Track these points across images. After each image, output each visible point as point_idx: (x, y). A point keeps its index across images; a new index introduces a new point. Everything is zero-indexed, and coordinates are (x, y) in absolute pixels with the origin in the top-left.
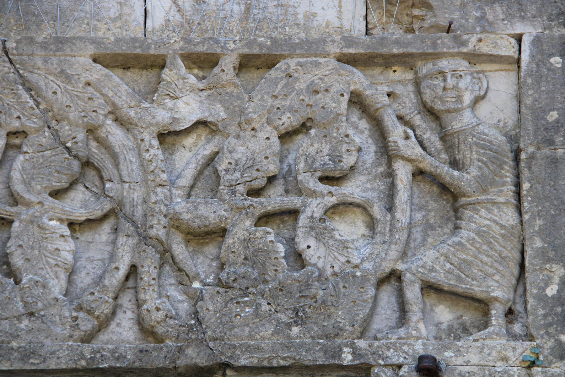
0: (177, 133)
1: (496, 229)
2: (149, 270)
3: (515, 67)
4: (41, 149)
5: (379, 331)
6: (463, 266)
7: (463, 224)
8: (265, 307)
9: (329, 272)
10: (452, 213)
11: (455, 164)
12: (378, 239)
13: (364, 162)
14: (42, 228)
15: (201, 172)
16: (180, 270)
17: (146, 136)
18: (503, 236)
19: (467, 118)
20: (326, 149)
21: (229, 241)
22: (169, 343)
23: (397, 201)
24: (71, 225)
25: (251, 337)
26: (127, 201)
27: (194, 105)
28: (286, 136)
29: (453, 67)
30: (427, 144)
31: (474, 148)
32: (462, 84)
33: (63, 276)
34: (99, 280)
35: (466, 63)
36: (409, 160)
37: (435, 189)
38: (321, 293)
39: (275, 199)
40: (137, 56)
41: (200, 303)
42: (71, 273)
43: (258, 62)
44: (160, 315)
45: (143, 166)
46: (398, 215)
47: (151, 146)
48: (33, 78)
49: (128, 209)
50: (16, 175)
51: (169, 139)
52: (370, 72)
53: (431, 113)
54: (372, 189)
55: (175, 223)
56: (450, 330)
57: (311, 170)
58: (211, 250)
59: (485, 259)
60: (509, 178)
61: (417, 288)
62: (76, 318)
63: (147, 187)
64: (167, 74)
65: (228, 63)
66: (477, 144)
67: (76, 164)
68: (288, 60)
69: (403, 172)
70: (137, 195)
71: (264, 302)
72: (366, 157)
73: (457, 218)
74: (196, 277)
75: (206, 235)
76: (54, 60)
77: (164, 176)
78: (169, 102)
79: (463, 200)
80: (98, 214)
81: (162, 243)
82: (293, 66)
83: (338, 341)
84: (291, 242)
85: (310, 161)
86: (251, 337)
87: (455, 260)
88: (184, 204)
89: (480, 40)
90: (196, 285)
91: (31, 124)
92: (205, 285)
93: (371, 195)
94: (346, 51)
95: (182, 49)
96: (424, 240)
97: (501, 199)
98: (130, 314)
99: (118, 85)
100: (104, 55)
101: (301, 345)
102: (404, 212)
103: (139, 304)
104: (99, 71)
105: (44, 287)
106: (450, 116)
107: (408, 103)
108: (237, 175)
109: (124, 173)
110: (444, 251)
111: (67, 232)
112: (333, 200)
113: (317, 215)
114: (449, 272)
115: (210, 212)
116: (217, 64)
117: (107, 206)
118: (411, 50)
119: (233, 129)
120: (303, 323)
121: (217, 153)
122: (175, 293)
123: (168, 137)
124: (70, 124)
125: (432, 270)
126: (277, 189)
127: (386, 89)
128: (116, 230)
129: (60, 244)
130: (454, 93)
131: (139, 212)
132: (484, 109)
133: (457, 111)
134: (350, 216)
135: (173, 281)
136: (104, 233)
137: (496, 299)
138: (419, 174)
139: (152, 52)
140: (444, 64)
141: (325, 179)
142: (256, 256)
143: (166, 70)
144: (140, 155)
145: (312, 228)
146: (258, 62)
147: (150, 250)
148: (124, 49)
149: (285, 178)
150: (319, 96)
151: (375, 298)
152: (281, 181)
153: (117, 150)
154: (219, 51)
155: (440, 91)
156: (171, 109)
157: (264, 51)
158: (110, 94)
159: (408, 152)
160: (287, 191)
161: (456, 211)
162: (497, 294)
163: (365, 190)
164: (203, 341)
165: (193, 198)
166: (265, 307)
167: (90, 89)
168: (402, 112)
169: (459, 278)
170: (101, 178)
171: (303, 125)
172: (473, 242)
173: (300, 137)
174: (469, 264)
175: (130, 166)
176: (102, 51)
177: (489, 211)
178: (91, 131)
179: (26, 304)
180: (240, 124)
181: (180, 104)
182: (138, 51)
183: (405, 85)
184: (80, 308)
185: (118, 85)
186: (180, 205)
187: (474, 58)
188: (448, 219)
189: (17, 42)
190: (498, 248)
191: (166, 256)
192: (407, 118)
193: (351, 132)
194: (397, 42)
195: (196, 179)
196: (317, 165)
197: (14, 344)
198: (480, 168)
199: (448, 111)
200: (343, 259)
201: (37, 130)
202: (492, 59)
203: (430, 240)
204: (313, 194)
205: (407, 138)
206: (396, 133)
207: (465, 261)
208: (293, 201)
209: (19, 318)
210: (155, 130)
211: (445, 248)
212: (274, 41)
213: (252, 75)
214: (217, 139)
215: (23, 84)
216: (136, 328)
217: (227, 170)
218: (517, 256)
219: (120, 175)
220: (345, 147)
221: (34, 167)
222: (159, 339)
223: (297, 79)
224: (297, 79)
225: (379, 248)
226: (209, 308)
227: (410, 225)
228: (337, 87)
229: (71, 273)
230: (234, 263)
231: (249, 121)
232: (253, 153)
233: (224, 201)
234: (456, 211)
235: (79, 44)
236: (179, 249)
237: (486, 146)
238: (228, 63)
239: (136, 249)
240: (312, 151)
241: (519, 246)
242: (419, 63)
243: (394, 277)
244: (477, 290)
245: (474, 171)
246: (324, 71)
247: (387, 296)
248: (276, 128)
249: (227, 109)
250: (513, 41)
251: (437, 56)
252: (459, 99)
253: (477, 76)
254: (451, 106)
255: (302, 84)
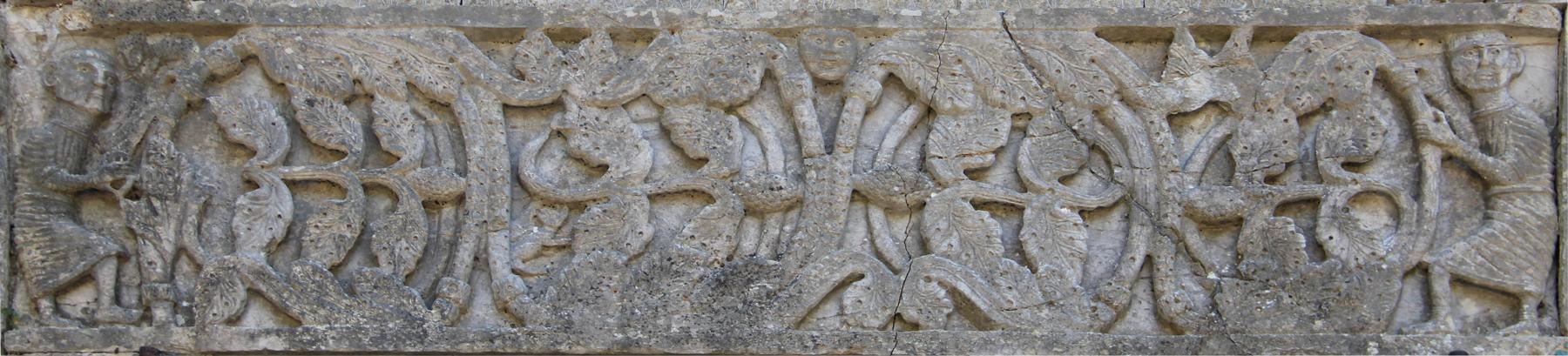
0: (1185, 114)
1: (1533, 220)
2: (1165, 261)
3: (1555, 40)
4: (1048, 132)
5: (1403, 324)
6: (1496, 259)
7: (1496, 214)
8: (1287, 300)
9: (1353, 264)
10: (1482, 202)
11: (1486, 148)
12: (1404, 229)
13: (1387, 146)
14: (1054, 216)
15: (1211, 157)
16: (1195, 260)
17: (1155, 117)
18: (1539, 227)
19: (1503, 98)
20: (1349, 132)
21: (1247, 231)
22: (1188, 334)
23: (1426, 190)
24: (1082, 212)
25: (1273, 330)
26: (1139, 188)
27: (1206, 83)
28: (1303, 118)
29: (1489, 41)
30: (1457, 126)
31: (1511, 132)
32: (1499, 61)
33: (1078, 266)
34: (1114, 271)
35: (1503, 37)
36: (1439, 145)
37: (1464, 175)
38: (1345, 286)
39: (1293, 187)
40: (1143, 29)
41: (1218, 295)
42: (1086, 261)
43: (1272, 35)
44: (1179, 307)
45: (1155, 150)
46: (1427, 205)
47: (1162, 129)
48: (1034, 54)
49: (1140, 196)
50: (1024, 160)
51: (1177, 121)
52: (1394, 46)
53: (1461, 91)
54: (1396, 176)
55: (1190, 212)
56: (1477, 323)
57: (1333, 155)
58: (1225, 239)
59: (1519, 251)
60: (1547, 166)
61: (1446, 281)
62: (1095, 309)
63: (1159, 173)
64: (1176, 49)
65: (1242, 36)
66: (1513, 128)
67: (1084, 147)
68: (1307, 33)
69: (1432, 157)
70: (1149, 181)
71: (1285, 295)
72: (1389, 140)
73: (1487, 207)
74: (1212, 268)
75: (1213, 225)
76: (1056, 35)
77: (1176, 162)
78: (1178, 80)
79: (1497, 189)
80: (1110, 201)
81: (1176, 232)
82: (1313, 40)
83: (1364, 335)
84: (1311, 232)
85: (1332, 146)
86: (1273, 330)
87: (1487, 253)
88: (1198, 191)
89: (1520, 11)
90: (1212, 276)
91: (1036, 105)
92: (1222, 276)
93: (1395, 182)
94: (1372, 22)
95: (1191, 20)
96: (1451, 231)
97: (1538, 188)
98: (1145, 305)
99: (1124, 62)
100: (1107, 29)
101: (1325, 339)
102: (1433, 201)
103: (1155, 295)
104: (1102, 48)
105: (1061, 277)
106: (1484, 96)
107: (1437, 80)
108: (1254, 160)
109: (1135, 158)
110: (1476, 242)
111: (1080, 221)
112: (1358, 188)
113: (1340, 204)
114: (1481, 265)
115: (1227, 201)
116: (1228, 37)
117: (1119, 193)
118: (1443, 22)
119: (1247, 110)
120: (1327, 316)
121: (1229, 136)
122: (1188, 283)
123: (1178, 118)
124: (1075, 105)
125: (1462, 263)
126: (1295, 174)
127: (1415, 65)
128: (1127, 218)
129: (1074, 233)
130: (1489, 71)
131: (1152, 199)
132: (1520, 88)
133: (1493, 90)
134: (1372, 204)
135: (1187, 271)
136: (1114, 221)
137: (1529, 293)
138: (1448, 159)
139: (1159, 24)
140: (1479, 37)
141: (1350, 165)
142: (1275, 247)
143: (1174, 45)
144: (1150, 139)
145: (1334, 218)
146: (1272, 35)
147: (1166, 240)
148: (1129, 21)
149: (1310, 167)
150: (1342, 74)
151: (1401, 291)
152: (1298, 166)
153: (1126, 133)
154: (1231, 22)
155: (1474, 69)
156: (1181, 88)
157: (1281, 23)
158: (1116, 72)
159: (1439, 137)
160: (1304, 177)
161: (1487, 199)
162: (1531, 288)
163: (1388, 177)
164: (1223, 333)
165: (1204, 185)
166: (1287, 300)
167: (1094, 66)
168: (1430, 91)
169: (1490, 271)
170: (1108, 163)
171: (1323, 106)
172: (1506, 233)
173: (1318, 118)
174: (1502, 257)
175: (1140, 150)
176: (1107, 24)
177: (1525, 200)
178: (1097, 112)
179: (1045, 293)
180: (1254, 105)
181: (1190, 82)
182: (1144, 24)
183: (1432, 60)
184: (1097, 298)
185: (1124, 62)
186: (1195, 194)
187: (1512, 30)
188: (1477, 209)
189: (1017, 15)
190: (1533, 239)
191: (1182, 248)
192: (1436, 97)
193: (1376, 114)
194: (1428, 13)
195: (1207, 164)
196: (1339, 150)
197: (1037, 333)
198: (1517, 154)
199: (1483, 91)
200: (1368, 251)
201: (1042, 112)
202: (1532, 31)
203: (1458, 230)
204: (1336, 181)
205: (1437, 120)
206: (1425, 115)
207: (1497, 253)
208: (1312, 189)
209: (1039, 307)
210: (1165, 111)
211: (1476, 240)
212: (1292, 12)
213: (1267, 49)
214: (1229, 120)
215: (1025, 62)
216: (1152, 318)
217: (1242, 156)
218: (1552, 248)
219: (1130, 161)
220: (1370, 130)
221: (1042, 152)
222: (1177, 331)
223: (1317, 54)
224: (1317, 54)
225: (1405, 239)
226: (1230, 299)
227: (1439, 215)
228: (1361, 64)
229: (1086, 261)
230: (1252, 255)
231: (1265, 102)
232: (1270, 136)
233: (1240, 188)
234: (1487, 199)
235: (1082, 16)
236: (1194, 239)
237: (1527, 131)
238: (1242, 36)
239: (1152, 240)
240: (1333, 134)
241: (1554, 238)
242: (1450, 36)
243: (1423, 270)
244: (1510, 283)
245: (1510, 158)
246: (1348, 45)
247: (1412, 291)
248: (1295, 109)
249: (1240, 87)
250: (1556, 11)
251: (1470, 28)
252: (1496, 77)
253: (1514, 51)
254: (1487, 85)
255: (1323, 61)
